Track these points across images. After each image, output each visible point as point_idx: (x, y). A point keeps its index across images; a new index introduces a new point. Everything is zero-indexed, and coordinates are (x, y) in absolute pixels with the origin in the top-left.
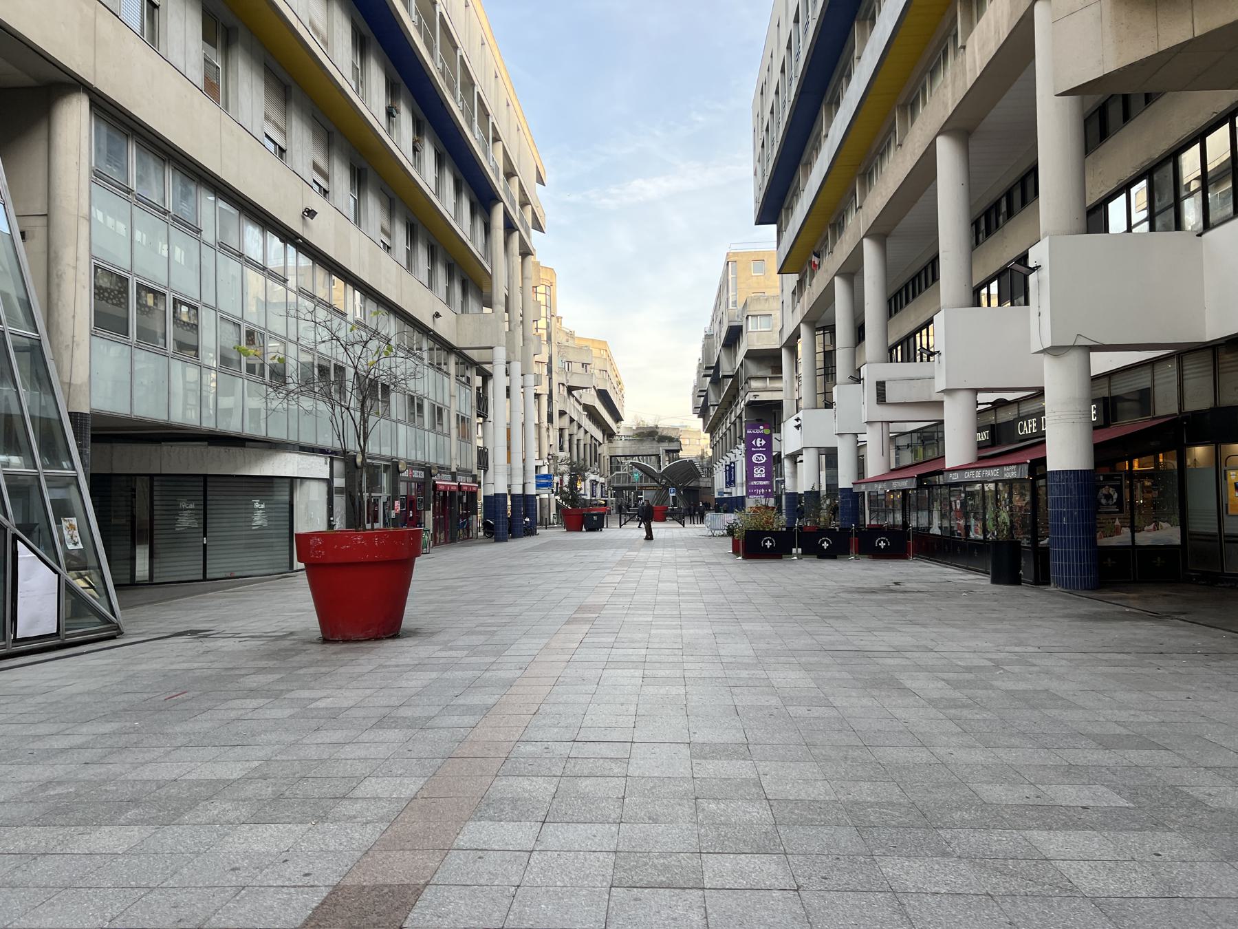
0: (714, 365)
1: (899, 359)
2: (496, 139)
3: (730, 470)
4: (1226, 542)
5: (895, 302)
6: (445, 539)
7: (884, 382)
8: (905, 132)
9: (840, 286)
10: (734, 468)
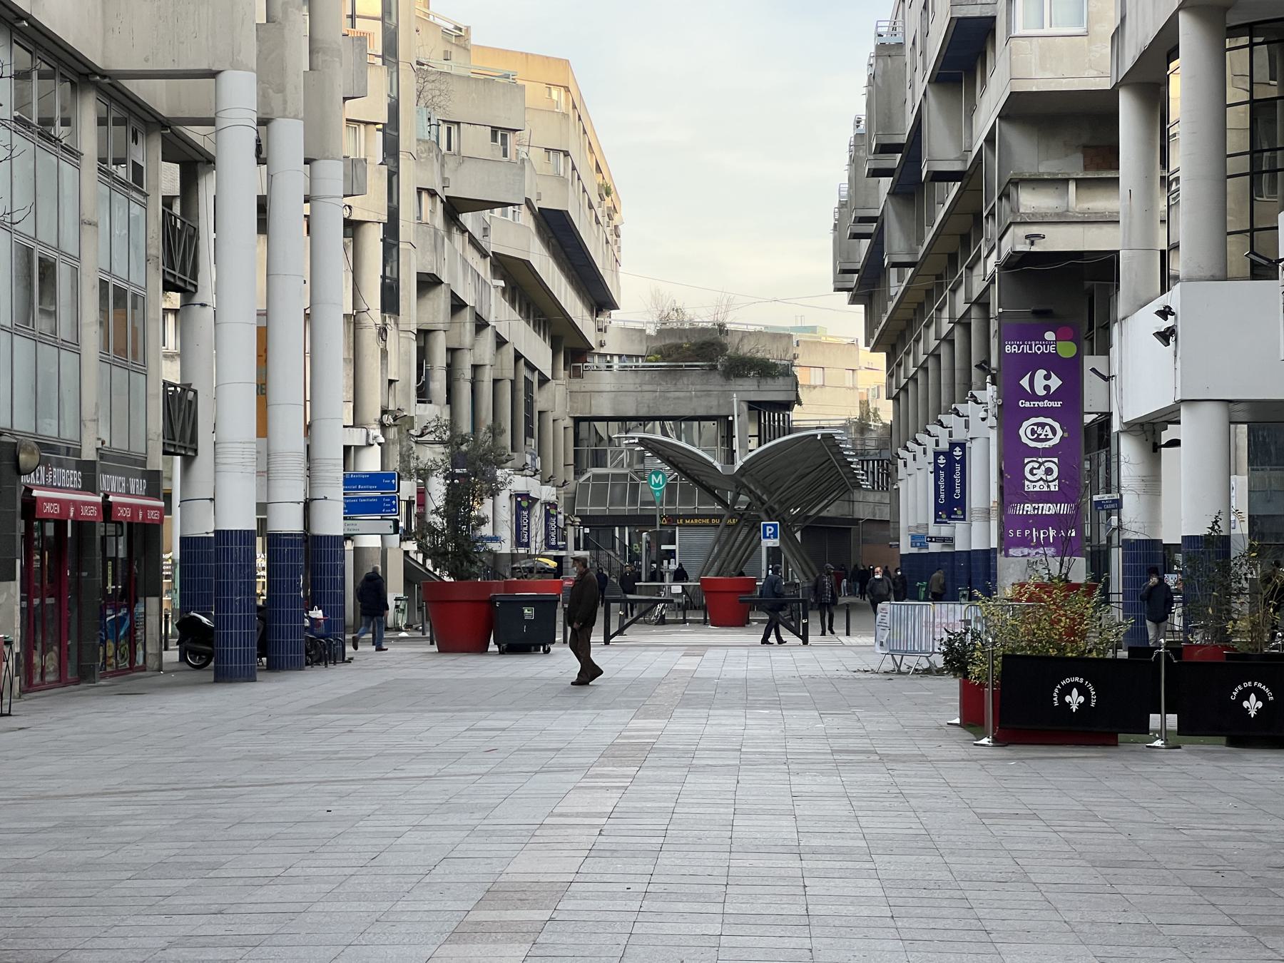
0: (903, 139)
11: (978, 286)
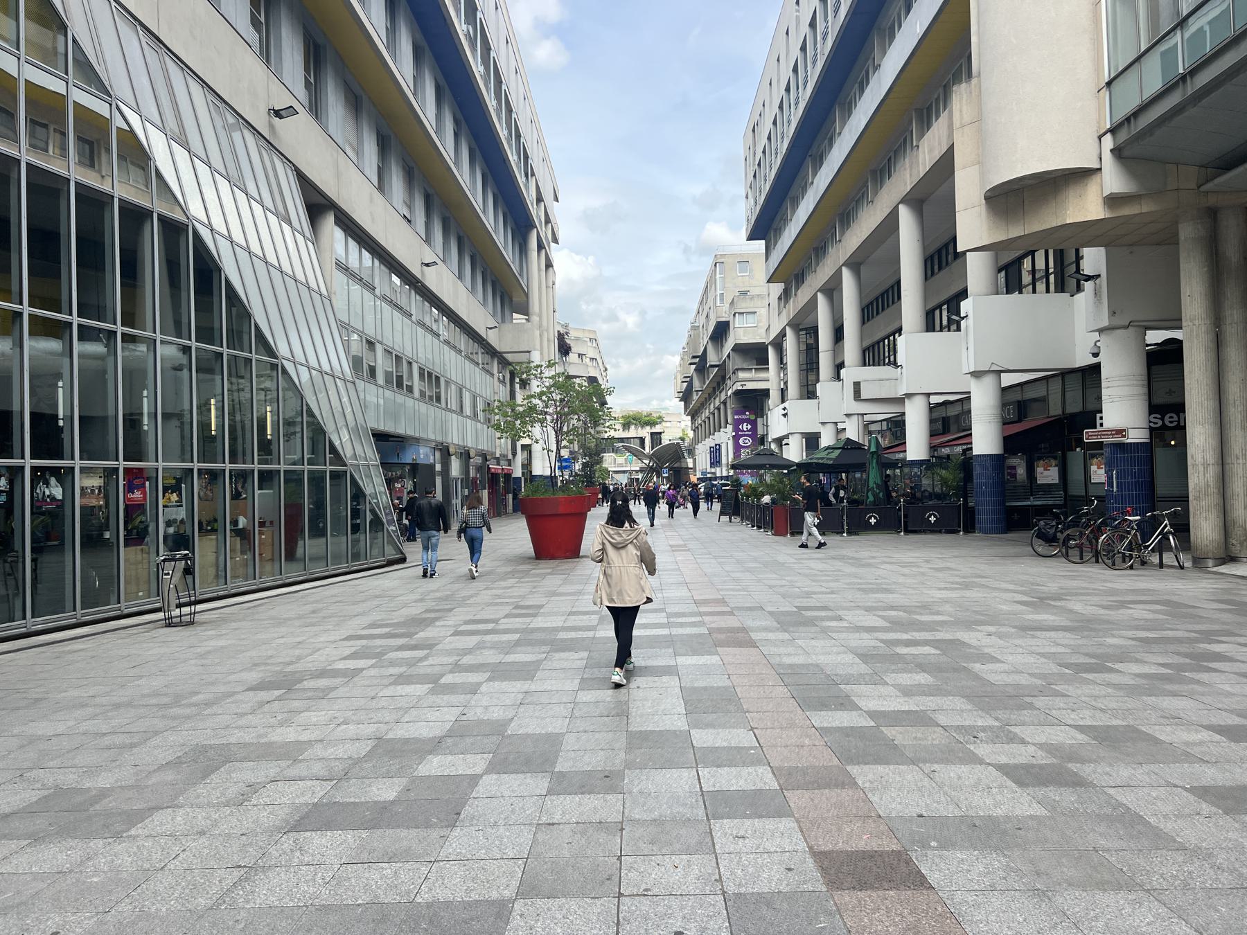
0: (700, 354)
1: (871, 363)
2: (533, 175)
3: (715, 452)
4: (1070, 500)
5: (868, 312)
6: (494, 514)
7: (859, 382)
8: (876, 193)
9: (822, 301)
10: (719, 449)
11: (723, 397)
